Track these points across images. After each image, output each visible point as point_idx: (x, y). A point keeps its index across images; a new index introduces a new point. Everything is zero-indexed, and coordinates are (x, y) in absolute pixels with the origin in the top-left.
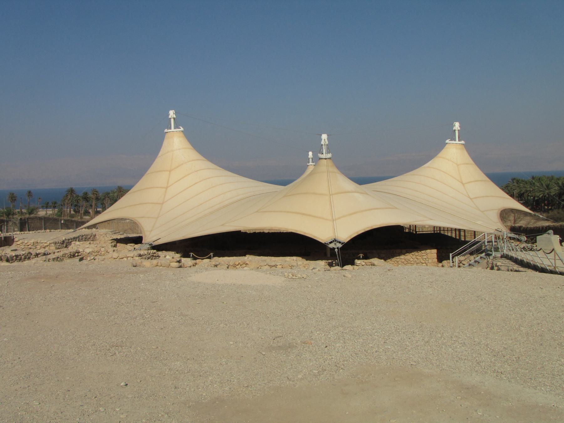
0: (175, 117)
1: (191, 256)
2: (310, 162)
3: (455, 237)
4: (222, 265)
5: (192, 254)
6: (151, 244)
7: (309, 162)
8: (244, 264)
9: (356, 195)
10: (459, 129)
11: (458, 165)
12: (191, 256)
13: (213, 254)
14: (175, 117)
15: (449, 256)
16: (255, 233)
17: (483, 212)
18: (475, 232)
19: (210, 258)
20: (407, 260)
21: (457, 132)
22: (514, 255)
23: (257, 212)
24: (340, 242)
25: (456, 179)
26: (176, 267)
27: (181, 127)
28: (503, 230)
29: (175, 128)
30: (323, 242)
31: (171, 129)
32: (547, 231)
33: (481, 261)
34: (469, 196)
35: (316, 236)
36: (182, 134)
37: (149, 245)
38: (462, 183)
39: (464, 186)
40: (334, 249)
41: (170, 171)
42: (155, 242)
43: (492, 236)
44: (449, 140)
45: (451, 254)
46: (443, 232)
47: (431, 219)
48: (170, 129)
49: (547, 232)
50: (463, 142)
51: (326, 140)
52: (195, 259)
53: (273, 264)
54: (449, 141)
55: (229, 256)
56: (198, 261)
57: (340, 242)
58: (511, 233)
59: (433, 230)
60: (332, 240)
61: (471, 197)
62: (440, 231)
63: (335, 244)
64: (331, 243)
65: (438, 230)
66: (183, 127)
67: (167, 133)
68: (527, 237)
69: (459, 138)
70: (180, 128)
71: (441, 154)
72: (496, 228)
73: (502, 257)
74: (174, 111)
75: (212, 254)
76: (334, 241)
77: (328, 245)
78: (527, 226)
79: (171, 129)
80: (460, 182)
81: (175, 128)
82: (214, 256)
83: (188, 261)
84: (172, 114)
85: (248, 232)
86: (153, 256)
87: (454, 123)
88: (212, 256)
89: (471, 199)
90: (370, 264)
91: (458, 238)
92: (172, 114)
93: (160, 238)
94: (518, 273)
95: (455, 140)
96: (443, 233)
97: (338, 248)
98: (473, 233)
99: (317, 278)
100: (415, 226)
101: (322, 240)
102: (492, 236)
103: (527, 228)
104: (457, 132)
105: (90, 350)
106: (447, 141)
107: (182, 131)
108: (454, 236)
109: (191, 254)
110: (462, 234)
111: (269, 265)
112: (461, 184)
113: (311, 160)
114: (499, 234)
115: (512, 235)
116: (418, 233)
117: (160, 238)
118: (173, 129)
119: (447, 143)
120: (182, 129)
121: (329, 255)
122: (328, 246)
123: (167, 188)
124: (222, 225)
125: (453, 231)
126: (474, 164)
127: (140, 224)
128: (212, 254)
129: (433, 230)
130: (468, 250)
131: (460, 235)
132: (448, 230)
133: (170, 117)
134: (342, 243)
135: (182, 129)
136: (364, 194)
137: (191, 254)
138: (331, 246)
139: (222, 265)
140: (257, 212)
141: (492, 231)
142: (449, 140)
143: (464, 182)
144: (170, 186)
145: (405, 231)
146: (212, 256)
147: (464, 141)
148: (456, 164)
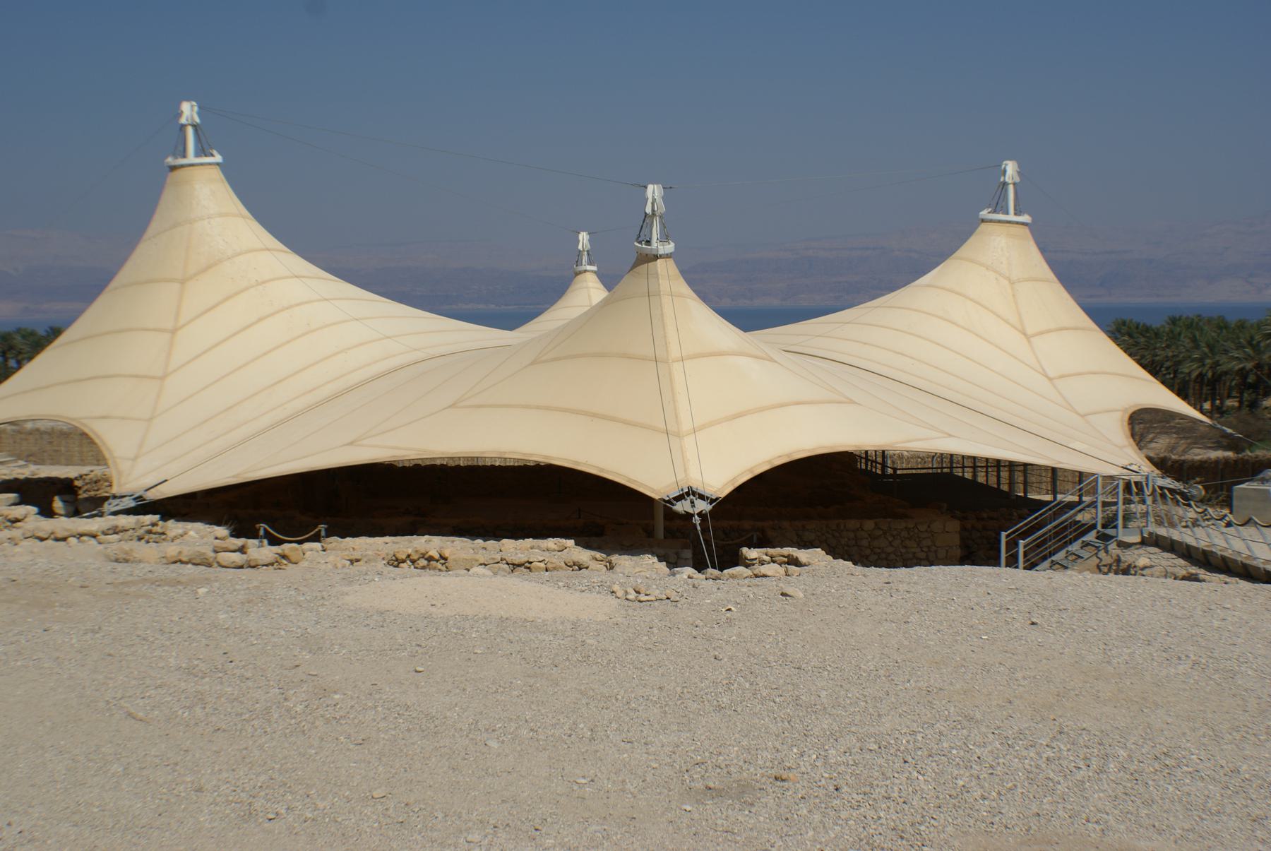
0: (197, 120)
1: (262, 532)
2: (584, 263)
3: (995, 486)
4: (369, 560)
5: (265, 529)
6: (140, 497)
7: (578, 263)
8: (423, 557)
9: (743, 361)
10: (1017, 180)
11: (1012, 283)
12: (262, 532)
13: (326, 530)
14: (197, 120)
15: (999, 541)
16: (417, 466)
17: (1083, 416)
18: (1054, 470)
19: (316, 538)
20: (879, 551)
21: (1011, 189)
22: (1191, 541)
23: (453, 406)
24: (702, 497)
25: (1007, 322)
26: (232, 566)
27: (215, 152)
28: (1142, 467)
29: (197, 155)
30: (657, 497)
31: (184, 156)
32: (1261, 472)
33: (1084, 553)
34: (1043, 370)
35: (52, 467)
36: (216, 173)
37: (135, 499)
38: (1025, 334)
39: (1029, 342)
40: (689, 516)
41: (183, 282)
42: (152, 490)
43: (1118, 484)
44: (990, 210)
45: (1004, 534)
46: (960, 470)
47: (950, 435)
48: (1003, 213)
49: (1261, 476)
50: (1026, 218)
51: (659, 201)
52: (274, 542)
53: (521, 558)
54: (989, 213)
55: (372, 534)
56: (286, 547)
57: (702, 497)
58: (1162, 478)
59: (949, 465)
60: (682, 490)
61: (1051, 374)
62: (951, 468)
63: (692, 502)
64: (679, 498)
65: (944, 465)
66: (220, 153)
67: (983, 226)
68: (1206, 488)
69: (1015, 209)
70: (212, 155)
71: (964, 251)
72: (1125, 462)
73: (1144, 542)
74: (194, 103)
75: (322, 527)
76: (688, 494)
77: (673, 505)
78: (1183, 458)
79: (184, 156)
80: (1020, 331)
81: (197, 155)
82: (329, 534)
83: (260, 551)
84: (189, 111)
85: (423, 465)
86: (150, 532)
87: (1005, 162)
88: (323, 533)
89: (1050, 379)
90: (786, 559)
91: (1005, 488)
92: (189, 111)
93: (166, 481)
94: (84, 589)
95: (1007, 213)
96: (960, 474)
97: (700, 514)
98: (1050, 475)
99: (709, 601)
100: (883, 452)
101: (653, 490)
102: (1118, 484)
103: (1184, 461)
104: (1011, 189)
105: (228, 801)
106: (984, 213)
107: (218, 164)
108: (993, 481)
109: (262, 529)
110: (1019, 477)
111: (509, 562)
112: (1023, 336)
113: (585, 258)
114: (1135, 478)
115: (1168, 482)
116: (899, 472)
117: (166, 481)
118: (191, 158)
119: (983, 221)
120: (218, 158)
121: (660, 532)
122: (671, 508)
123: (174, 331)
124: (351, 443)
125: (990, 469)
126: (1055, 279)
127: (98, 437)
128: (322, 527)
129: (949, 465)
130: (1051, 523)
131: (1011, 483)
132: (987, 467)
133: (183, 121)
134: (712, 501)
135: (218, 158)
136: (763, 359)
137: (262, 529)
138: (680, 507)
139: (369, 560)
140: (453, 406)
141: (1114, 471)
142: (990, 210)
143: (1029, 331)
144: (184, 326)
145: (859, 466)
146: (323, 533)
147: (1030, 215)
148: (1010, 280)
